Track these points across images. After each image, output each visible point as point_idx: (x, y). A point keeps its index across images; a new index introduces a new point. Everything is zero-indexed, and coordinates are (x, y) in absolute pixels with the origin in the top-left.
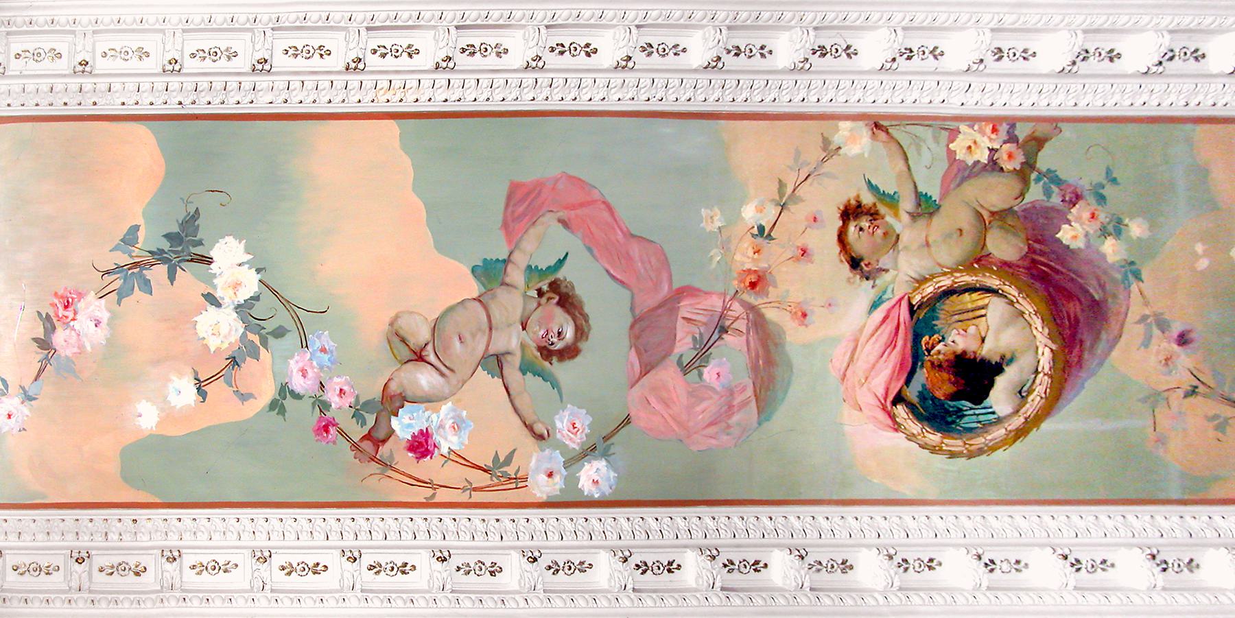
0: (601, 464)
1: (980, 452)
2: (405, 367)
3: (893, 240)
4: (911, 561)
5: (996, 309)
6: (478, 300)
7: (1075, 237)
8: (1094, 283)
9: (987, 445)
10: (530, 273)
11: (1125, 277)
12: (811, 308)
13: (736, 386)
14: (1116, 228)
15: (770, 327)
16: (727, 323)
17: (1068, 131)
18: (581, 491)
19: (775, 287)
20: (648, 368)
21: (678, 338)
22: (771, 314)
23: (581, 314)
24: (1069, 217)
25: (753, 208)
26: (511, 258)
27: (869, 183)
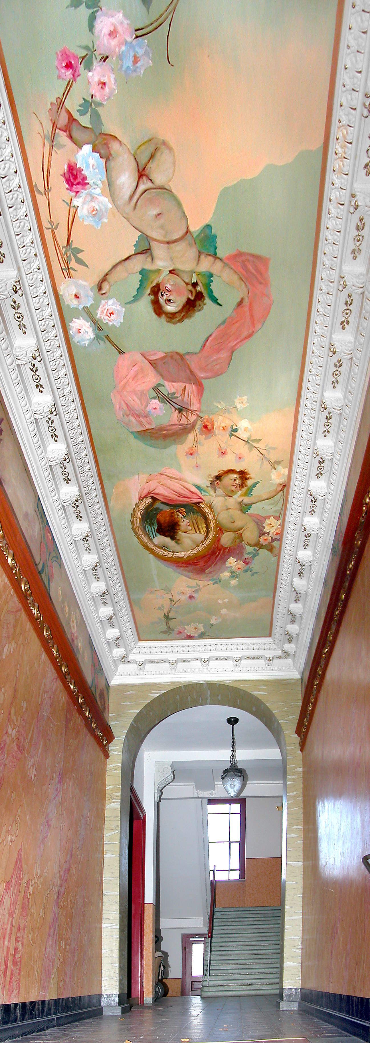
0: (91, 335)
1: (136, 533)
2: (133, 157)
3: (230, 494)
4: (78, 509)
5: (199, 537)
6: (188, 231)
7: (230, 563)
8: (212, 570)
9: (139, 535)
10: (208, 276)
11: (214, 579)
12: (195, 457)
13: (150, 419)
14: (234, 575)
15: (184, 437)
16: (184, 413)
17: (274, 559)
18: (71, 321)
19: (205, 439)
20: (154, 365)
21: (173, 383)
22: (191, 437)
23: (183, 316)
24: (239, 561)
25: (246, 426)
26: (218, 260)
27: (257, 483)
